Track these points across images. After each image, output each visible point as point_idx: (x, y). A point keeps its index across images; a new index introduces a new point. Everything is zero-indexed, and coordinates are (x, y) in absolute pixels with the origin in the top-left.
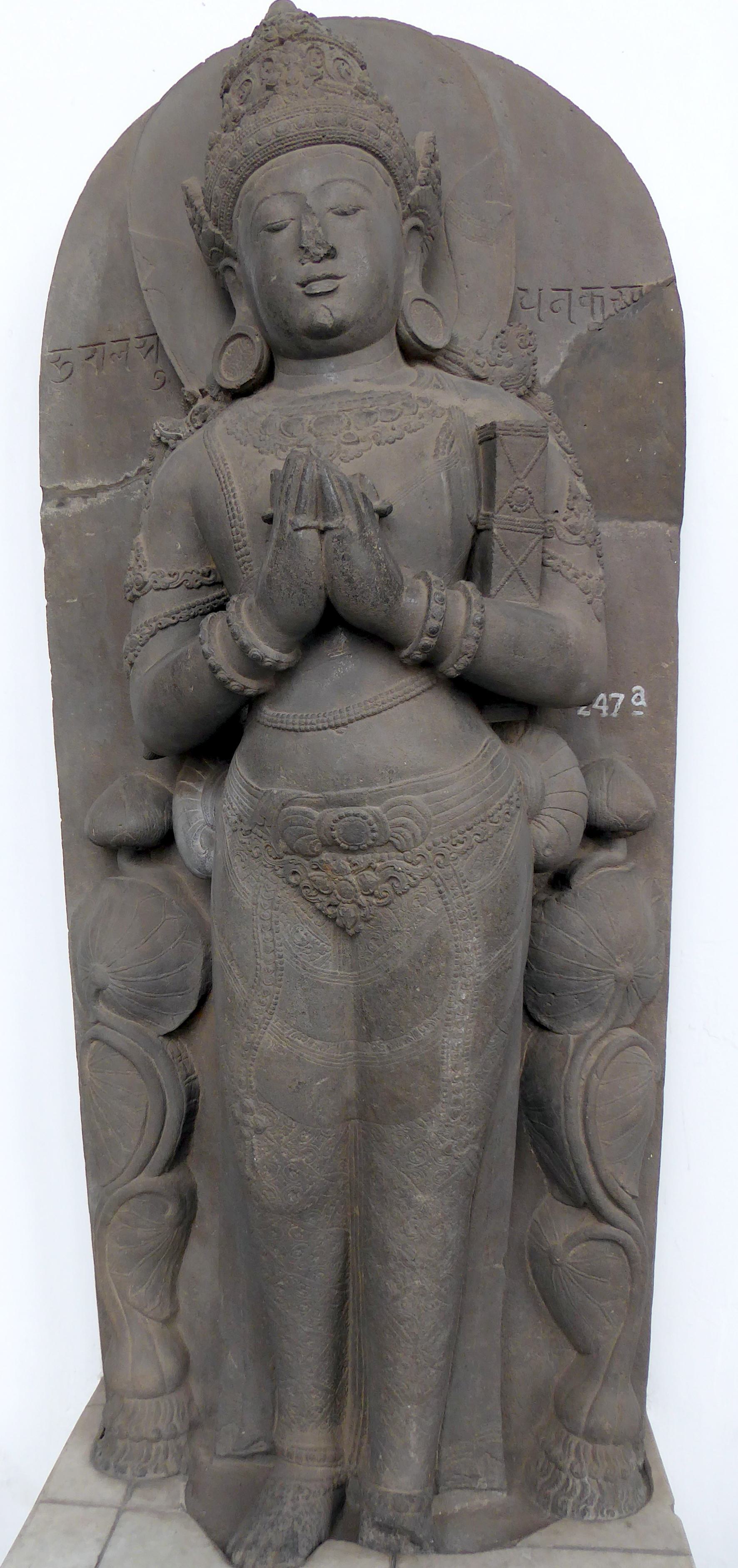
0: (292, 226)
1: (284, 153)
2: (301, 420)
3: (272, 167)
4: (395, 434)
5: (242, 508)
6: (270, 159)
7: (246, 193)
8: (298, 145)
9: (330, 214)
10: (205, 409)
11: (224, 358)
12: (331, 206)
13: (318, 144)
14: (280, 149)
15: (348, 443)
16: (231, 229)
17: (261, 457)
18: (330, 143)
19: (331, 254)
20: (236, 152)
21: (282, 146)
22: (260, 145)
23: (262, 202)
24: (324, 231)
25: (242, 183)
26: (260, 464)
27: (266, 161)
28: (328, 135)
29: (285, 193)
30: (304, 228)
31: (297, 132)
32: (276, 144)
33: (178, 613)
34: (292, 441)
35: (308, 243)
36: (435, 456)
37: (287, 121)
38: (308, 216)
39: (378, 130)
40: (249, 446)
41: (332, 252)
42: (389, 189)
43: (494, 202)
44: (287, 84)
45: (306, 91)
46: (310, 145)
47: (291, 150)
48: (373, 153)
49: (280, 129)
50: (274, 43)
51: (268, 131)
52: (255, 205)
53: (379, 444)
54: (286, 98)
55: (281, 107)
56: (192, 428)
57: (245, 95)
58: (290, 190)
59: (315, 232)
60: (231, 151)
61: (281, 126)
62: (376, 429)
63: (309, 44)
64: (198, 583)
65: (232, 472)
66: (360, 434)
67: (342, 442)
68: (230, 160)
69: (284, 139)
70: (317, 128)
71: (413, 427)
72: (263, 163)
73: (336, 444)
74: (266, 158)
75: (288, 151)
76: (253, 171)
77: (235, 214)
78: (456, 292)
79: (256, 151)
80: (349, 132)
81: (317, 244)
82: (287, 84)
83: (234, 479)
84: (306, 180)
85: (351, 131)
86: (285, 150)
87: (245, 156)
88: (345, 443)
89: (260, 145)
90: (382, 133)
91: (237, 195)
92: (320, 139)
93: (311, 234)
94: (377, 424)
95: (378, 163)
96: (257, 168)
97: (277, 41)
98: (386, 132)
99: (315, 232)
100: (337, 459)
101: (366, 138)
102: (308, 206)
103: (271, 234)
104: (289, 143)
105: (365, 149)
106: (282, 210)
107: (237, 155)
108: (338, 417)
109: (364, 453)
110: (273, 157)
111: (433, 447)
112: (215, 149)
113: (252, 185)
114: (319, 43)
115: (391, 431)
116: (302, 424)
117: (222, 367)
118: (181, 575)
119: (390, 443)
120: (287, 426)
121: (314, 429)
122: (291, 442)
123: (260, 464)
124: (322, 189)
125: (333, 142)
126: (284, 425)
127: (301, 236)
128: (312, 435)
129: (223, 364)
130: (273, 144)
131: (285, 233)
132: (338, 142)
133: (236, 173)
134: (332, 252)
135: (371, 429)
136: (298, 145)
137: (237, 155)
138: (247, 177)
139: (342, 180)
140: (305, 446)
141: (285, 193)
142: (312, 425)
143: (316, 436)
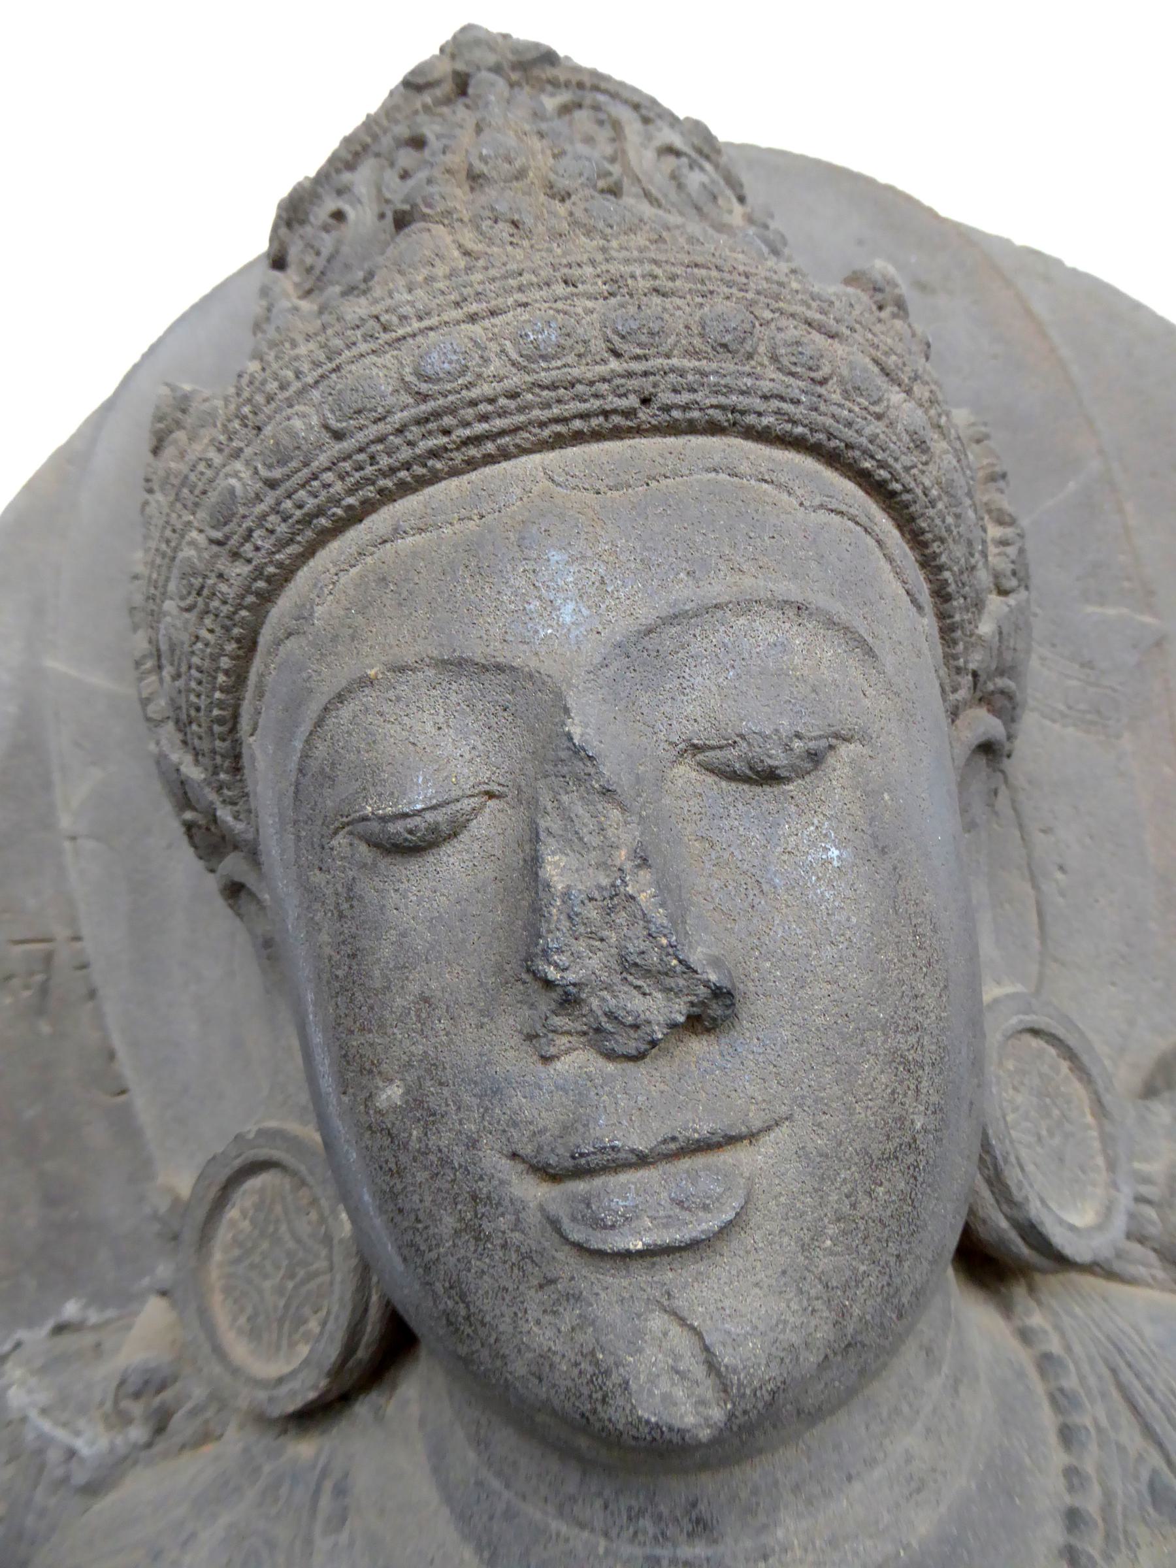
0: (490, 826)
1: (454, 472)
3: (398, 532)
6: (387, 497)
7: (278, 643)
8: (522, 438)
9: (686, 773)
10: (162, 1387)
11: (223, 1234)
12: (700, 733)
13: (617, 433)
14: (434, 454)
16: (237, 769)
18: (673, 429)
19: (711, 1012)
20: (238, 465)
21: (451, 438)
22: (338, 436)
23: (340, 698)
24: (666, 890)
25: (267, 598)
27: (368, 508)
28: (666, 397)
29: (456, 666)
30: (557, 868)
31: (516, 380)
32: (415, 432)
35: (579, 962)
37: (476, 329)
38: (571, 800)
39: (881, 381)
41: (716, 1010)
42: (925, 621)
43: (1111, 612)
44: (475, 179)
45: (561, 209)
46: (578, 438)
47: (489, 460)
48: (863, 478)
49: (436, 363)
50: (438, 92)
51: (380, 374)
52: (313, 709)
54: (468, 238)
55: (441, 270)
57: (320, 263)
58: (478, 652)
59: (615, 899)
60: (217, 459)
61: (442, 350)
63: (564, 97)
68: (213, 497)
69: (452, 411)
70: (614, 364)
72: (355, 517)
74: (369, 492)
75: (472, 464)
76: (310, 551)
77: (245, 724)
78: (1027, 887)
79: (323, 459)
80: (766, 386)
81: (628, 966)
82: (475, 179)
84: (565, 614)
85: (771, 379)
86: (458, 457)
87: (272, 484)
89: (338, 436)
90: (896, 396)
91: (249, 645)
92: (629, 413)
93: (592, 912)
95: (884, 523)
96: (326, 536)
97: (448, 87)
98: (909, 392)
99: (615, 899)
101: (835, 412)
102: (577, 751)
103: (384, 863)
104: (480, 428)
105: (833, 458)
106: (435, 753)
107: (239, 478)
110: (405, 489)
112: (169, 451)
113: (303, 615)
114: (602, 98)
117: (214, 1275)
124: (645, 653)
125: (692, 428)
127: (537, 910)
129: (218, 1256)
130: (400, 431)
131: (453, 863)
132: (714, 428)
133: (235, 555)
134: (716, 1010)
136: (522, 438)
137: (239, 478)
138: (288, 573)
139: (746, 605)
141: (456, 666)
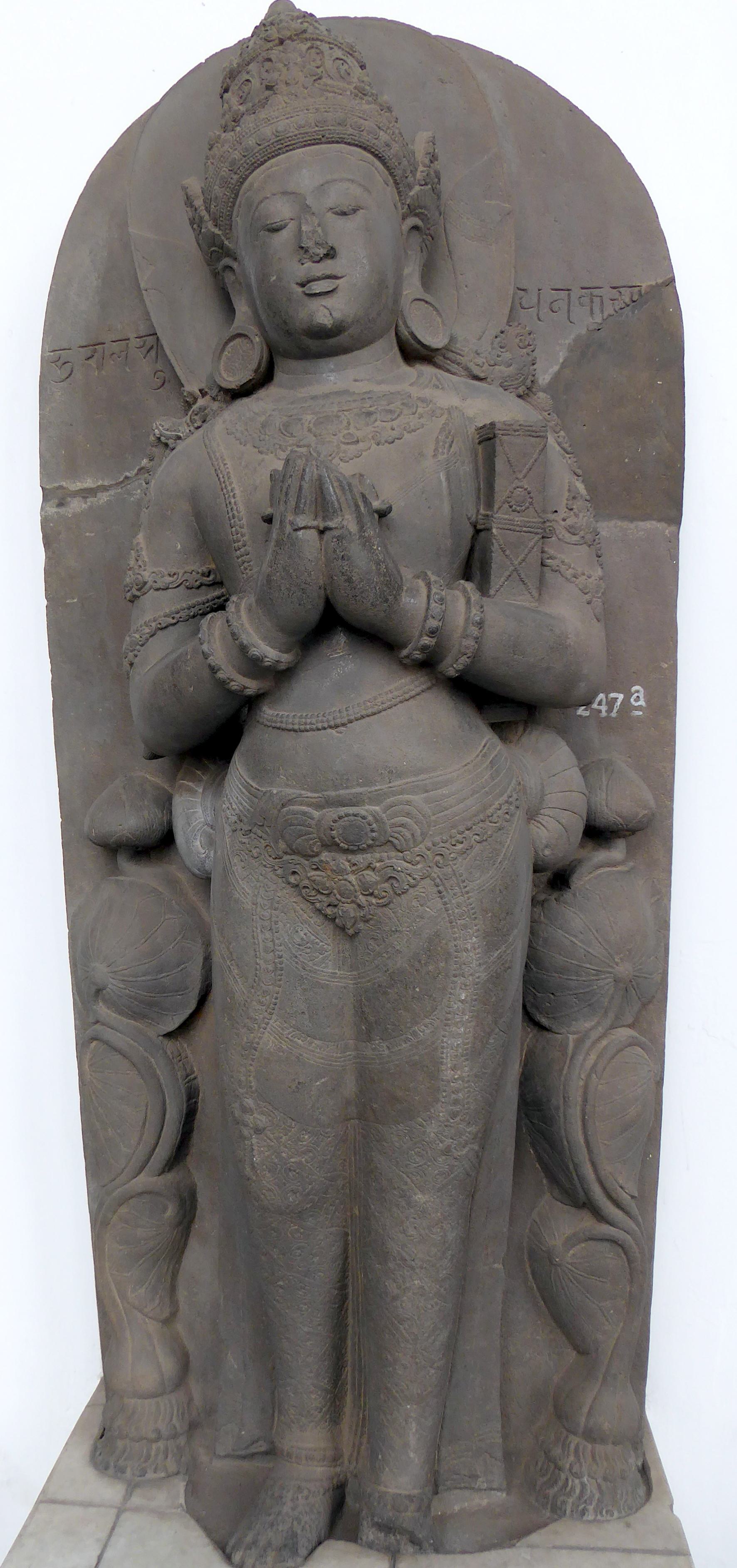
0: (292, 226)
1: (284, 153)
2: (300, 420)
3: (272, 167)
4: (395, 434)
5: (241, 508)
6: (269, 159)
7: (245, 193)
8: (297, 145)
9: (330, 214)
10: (205, 409)
11: (224, 358)
12: (331, 206)
13: (317, 144)
14: (279, 149)
15: (348, 443)
16: (231, 229)
17: (261, 457)
18: (329, 143)
19: (331, 254)
20: (236, 152)
21: (282, 146)
22: (259, 145)
23: (262, 202)
24: (323, 231)
25: (242, 183)
26: (259, 464)
27: (265, 161)
28: (327, 135)
29: (285, 193)
30: (304, 228)
31: (297, 132)
32: (275, 144)
33: (178, 613)
34: (291, 441)
35: (308, 243)
36: (435, 456)
37: (287, 121)
38: (308, 216)
39: (378, 130)
40: (249, 446)
41: (332, 252)
42: (389, 189)
43: (493, 202)
44: (287, 84)
45: (306, 91)
46: (309, 145)
47: (291, 150)
48: (372, 153)
49: (279, 129)
50: (274, 43)
51: (268, 131)
52: (255, 205)
53: (378, 444)
54: (286, 98)
55: (280, 107)
56: (192, 428)
57: (244, 95)
58: (289, 190)
59: (314, 232)
60: (231, 151)
61: (281, 126)
62: (376, 429)
63: (309, 44)
64: (198, 583)
65: (231, 472)
66: (359, 434)
67: (342, 442)
68: (230, 160)
69: (283, 139)
70: (317, 128)
71: (413, 427)
72: (262, 163)
73: (335, 444)
74: (266, 158)
75: (287, 151)
76: (253, 171)
77: (235, 214)
78: (455, 292)
79: (256, 151)
80: (348, 132)
81: (317, 244)
82: (287, 84)
83: (234, 479)
84: (306, 180)
85: (351, 131)
86: (284, 150)
87: (244, 156)
88: (344, 443)
89: (259, 145)
90: (382, 133)
91: (237, 195)
92: (320, 139)
93: (310, 234)
94: (377, 424)
95: (378, 163)
96: (256, 168)
97: (277, 41)
98: (386, 132)
99: (314, 232)
100: (337, 459)
101: (365, 138)
102: (307, 206)
103: (271, 234)
104: (289, 143)
105: (365, 149)
106: (281, 210)
107: (236, 155)
108: (338, 417)
109: (364, 453)
110: (273, 157)
111: (432, 447)
112: (215, 149)
113: (251, 185)
114: (318, 43)
115: (390, 431)
116: (302, 424)
117: (222, 367)
118: (180, 575)
119: (390, 443)
120: (286, 426)
121: (314, 429)
122: (291, 442)
123: (259, 464)
124: (322, 189)
125: (333, 142)
126: (284, 425)
127: (301, 236)
128: (312, 435)
129: (222, 364)
130: (272, 144)
131: (284, 233)
132: (338, 142)
133: (235, 173)
134: (332, 252)
135: (370, 429)
136: (297, 145)
137: (236, 155)
138: (247, 177)
139: (341, 180)
140: (304, 446)
141: (285, 193)
142: (311, 425)
143: (315, 436)
